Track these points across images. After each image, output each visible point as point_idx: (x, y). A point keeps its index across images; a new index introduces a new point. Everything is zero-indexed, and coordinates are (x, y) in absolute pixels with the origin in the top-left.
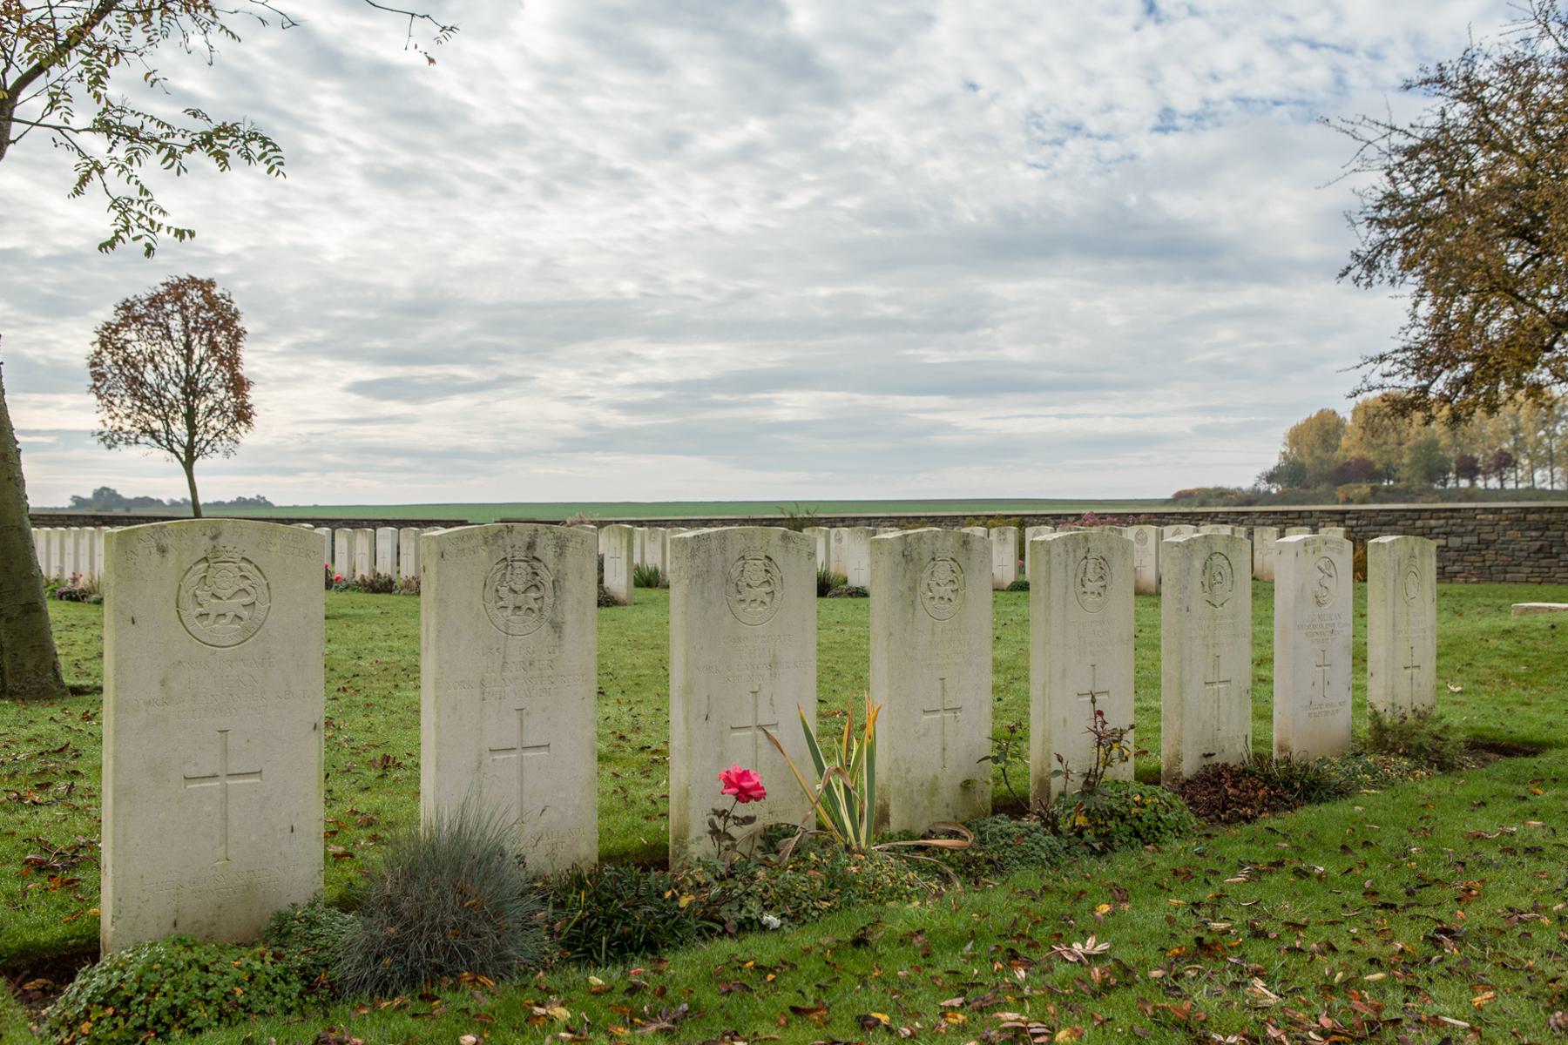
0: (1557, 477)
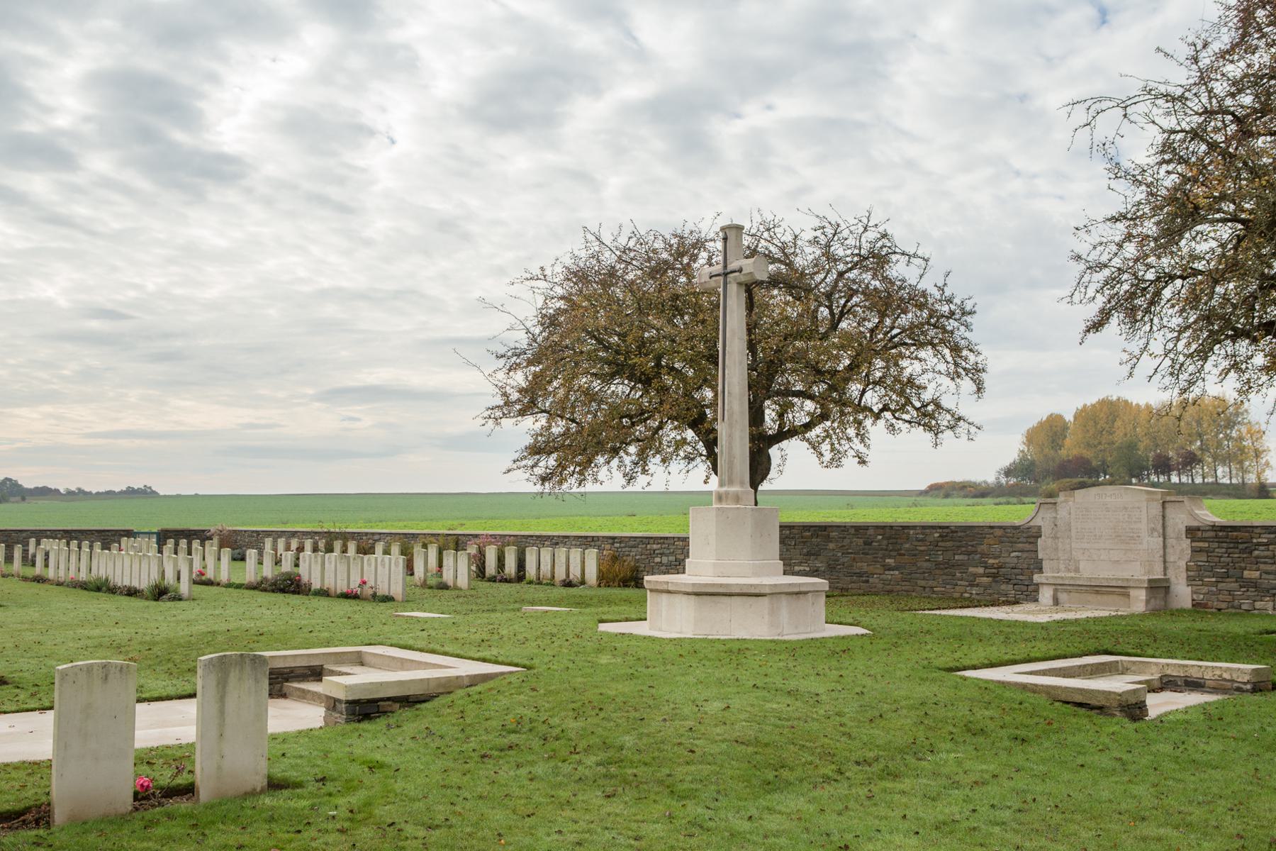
0: (1234, 472)
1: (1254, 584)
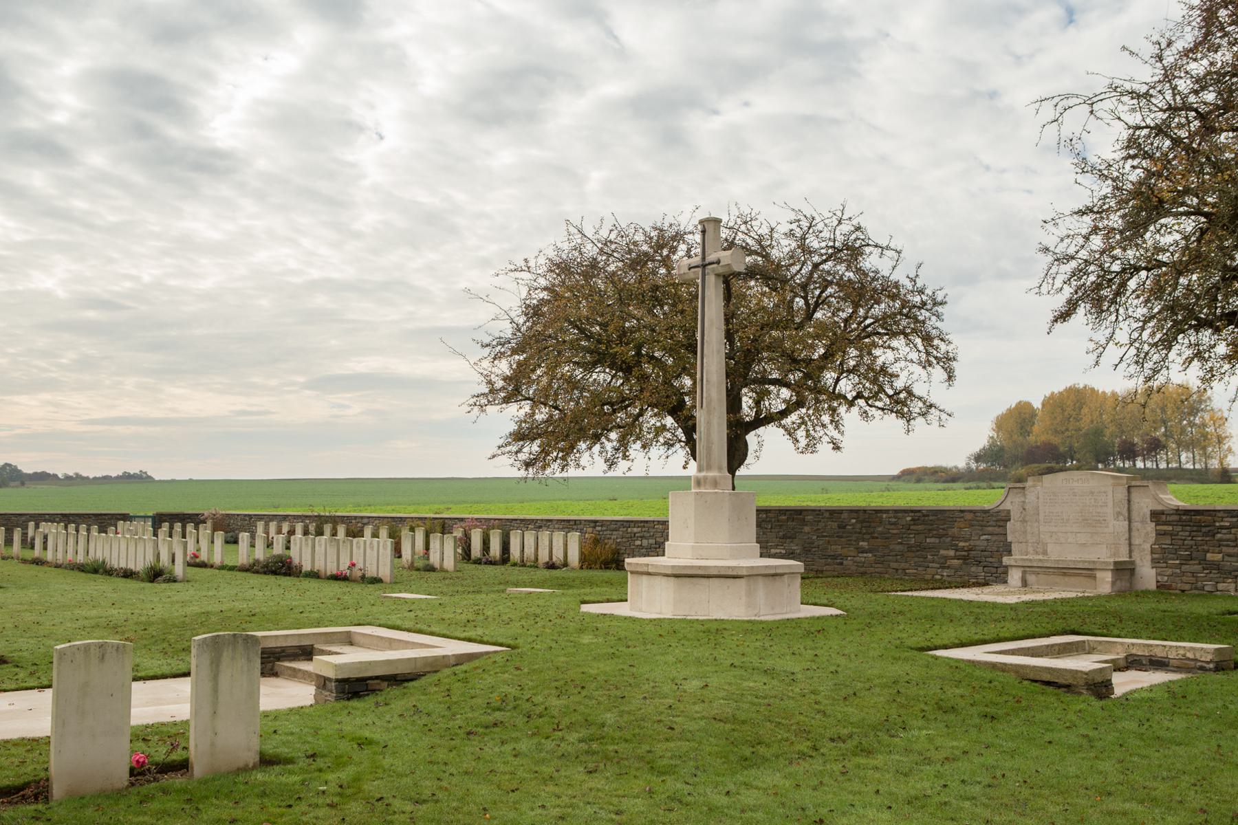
0: (1197, 458)
1: (1215, 566)
